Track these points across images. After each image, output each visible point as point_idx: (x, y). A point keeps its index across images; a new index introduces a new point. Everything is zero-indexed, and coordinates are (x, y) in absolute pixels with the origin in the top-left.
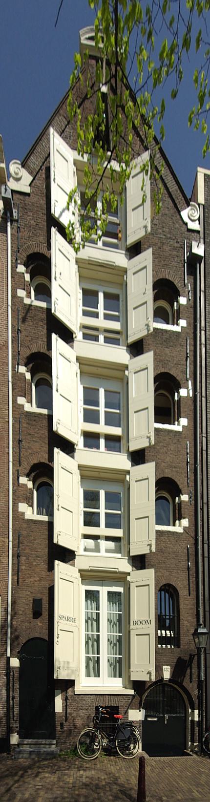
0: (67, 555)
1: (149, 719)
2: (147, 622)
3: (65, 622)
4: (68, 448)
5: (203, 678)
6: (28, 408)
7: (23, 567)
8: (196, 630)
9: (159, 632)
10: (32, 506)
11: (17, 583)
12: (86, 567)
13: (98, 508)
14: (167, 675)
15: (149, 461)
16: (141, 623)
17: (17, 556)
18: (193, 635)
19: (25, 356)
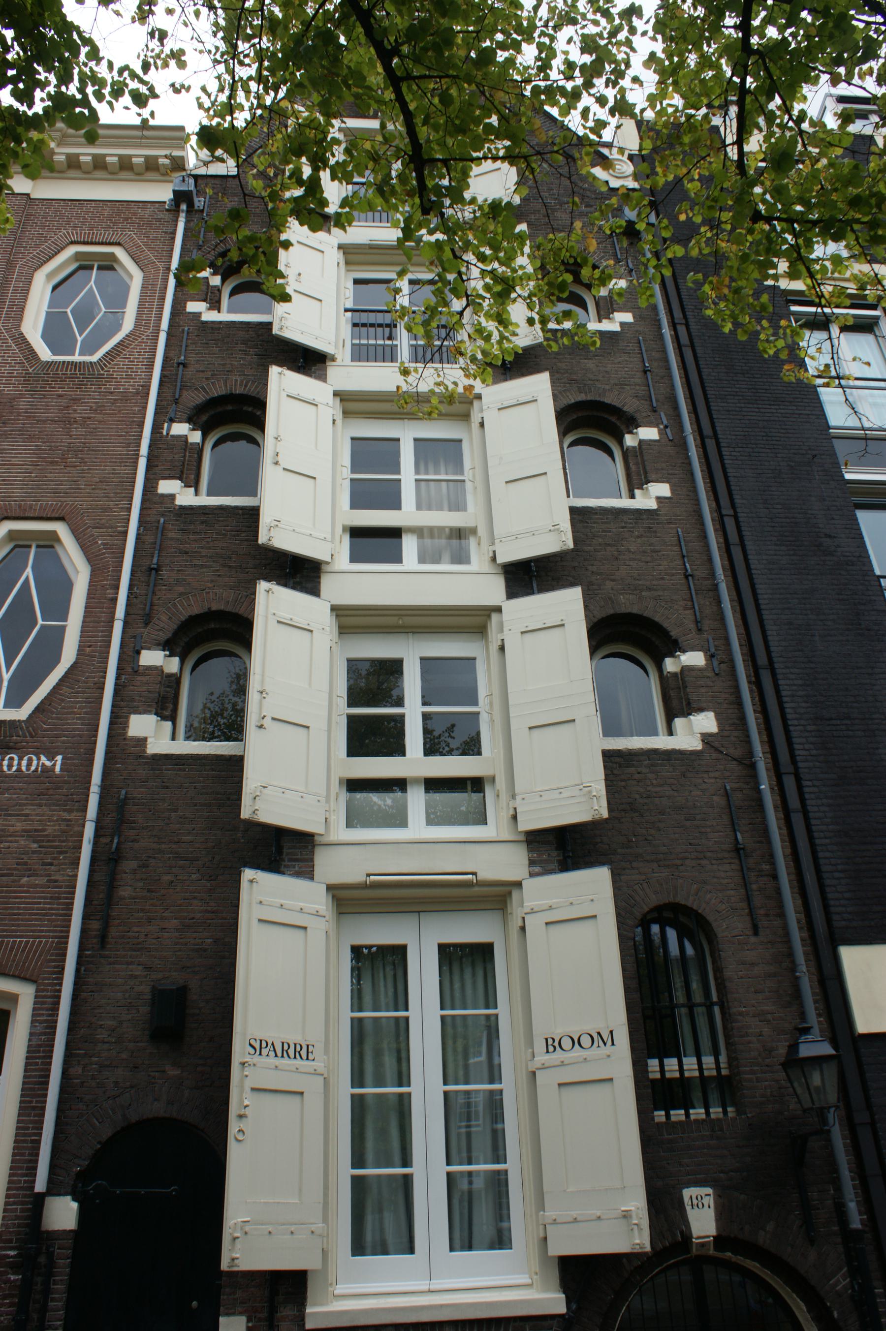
0: (285, 849)
1: (624, 1260)
2: (597, 1038)
3: (272, 1061)
4: (301, 573)
5: (856, 1222)
6: (186, 497)
7: (125, 892)
8: (794, 1047)
9: (653, 1064)
10: (173, 719)
11: (96, 941)
12: (355, 875)
13: (476, 703)
14: (702, 1220)
15: (554, 1257)
16: (576, 1042)
17: (106, 860)
18: (786, 1065)
19: (192, 404)
